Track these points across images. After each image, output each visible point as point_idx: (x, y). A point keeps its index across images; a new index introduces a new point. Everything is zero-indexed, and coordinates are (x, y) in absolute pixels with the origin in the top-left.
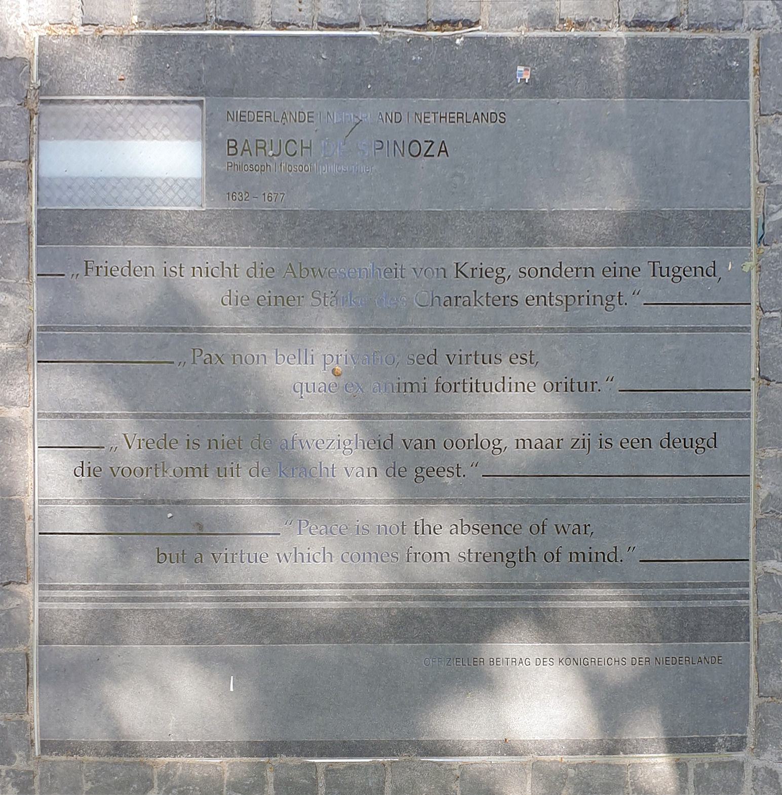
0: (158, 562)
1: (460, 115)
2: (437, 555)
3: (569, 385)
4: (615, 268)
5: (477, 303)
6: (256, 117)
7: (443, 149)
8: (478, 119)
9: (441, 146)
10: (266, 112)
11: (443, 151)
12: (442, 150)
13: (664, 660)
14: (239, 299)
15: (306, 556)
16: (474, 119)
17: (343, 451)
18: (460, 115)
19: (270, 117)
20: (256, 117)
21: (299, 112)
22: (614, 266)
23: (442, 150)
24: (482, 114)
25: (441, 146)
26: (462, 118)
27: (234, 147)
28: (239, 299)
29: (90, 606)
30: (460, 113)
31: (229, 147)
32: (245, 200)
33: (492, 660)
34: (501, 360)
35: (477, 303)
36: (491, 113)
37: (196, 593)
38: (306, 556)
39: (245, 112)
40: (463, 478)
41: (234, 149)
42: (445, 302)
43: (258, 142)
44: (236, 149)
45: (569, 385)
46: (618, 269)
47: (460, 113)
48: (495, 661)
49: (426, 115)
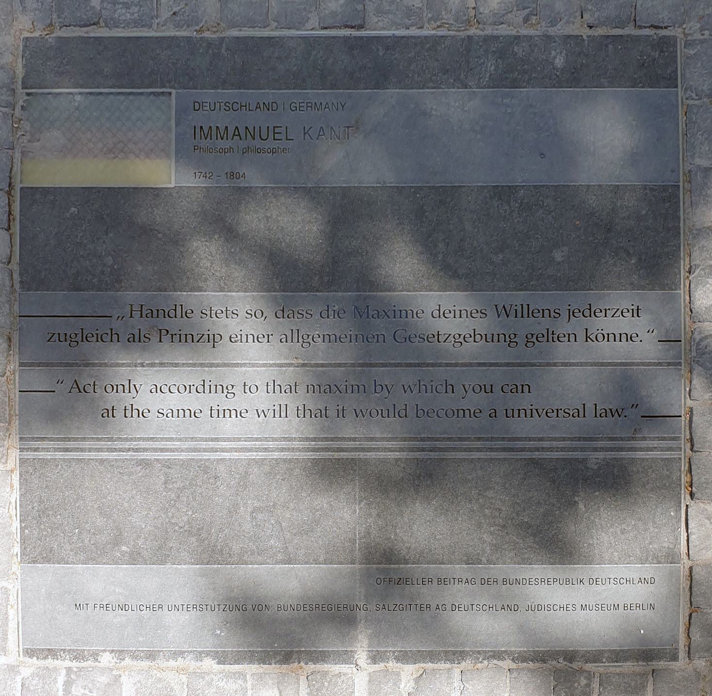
0: (417, 416)
1: (310, 105)
6: (201, 106)
7: (237, 133)
8: (260, 108)
9: (320, 130)
10: (307, 103)
11: (237, 135)
12: (236, 134)
15: (429, 387)
16: (257, 108)
17: (226, 395)
19: (311, 107)
20: (201, 106)
21: (272, 103)
23: (236, 134)
24: (264, 103)
25: (320, 130)
29: (412, 455)
34: (202, 312)
36: (272, 103)
37: (386, 444)
38: (429, 387)
39: (207, 102)
43: (276, 129)
48: (443, 581)
49: (301, 104)
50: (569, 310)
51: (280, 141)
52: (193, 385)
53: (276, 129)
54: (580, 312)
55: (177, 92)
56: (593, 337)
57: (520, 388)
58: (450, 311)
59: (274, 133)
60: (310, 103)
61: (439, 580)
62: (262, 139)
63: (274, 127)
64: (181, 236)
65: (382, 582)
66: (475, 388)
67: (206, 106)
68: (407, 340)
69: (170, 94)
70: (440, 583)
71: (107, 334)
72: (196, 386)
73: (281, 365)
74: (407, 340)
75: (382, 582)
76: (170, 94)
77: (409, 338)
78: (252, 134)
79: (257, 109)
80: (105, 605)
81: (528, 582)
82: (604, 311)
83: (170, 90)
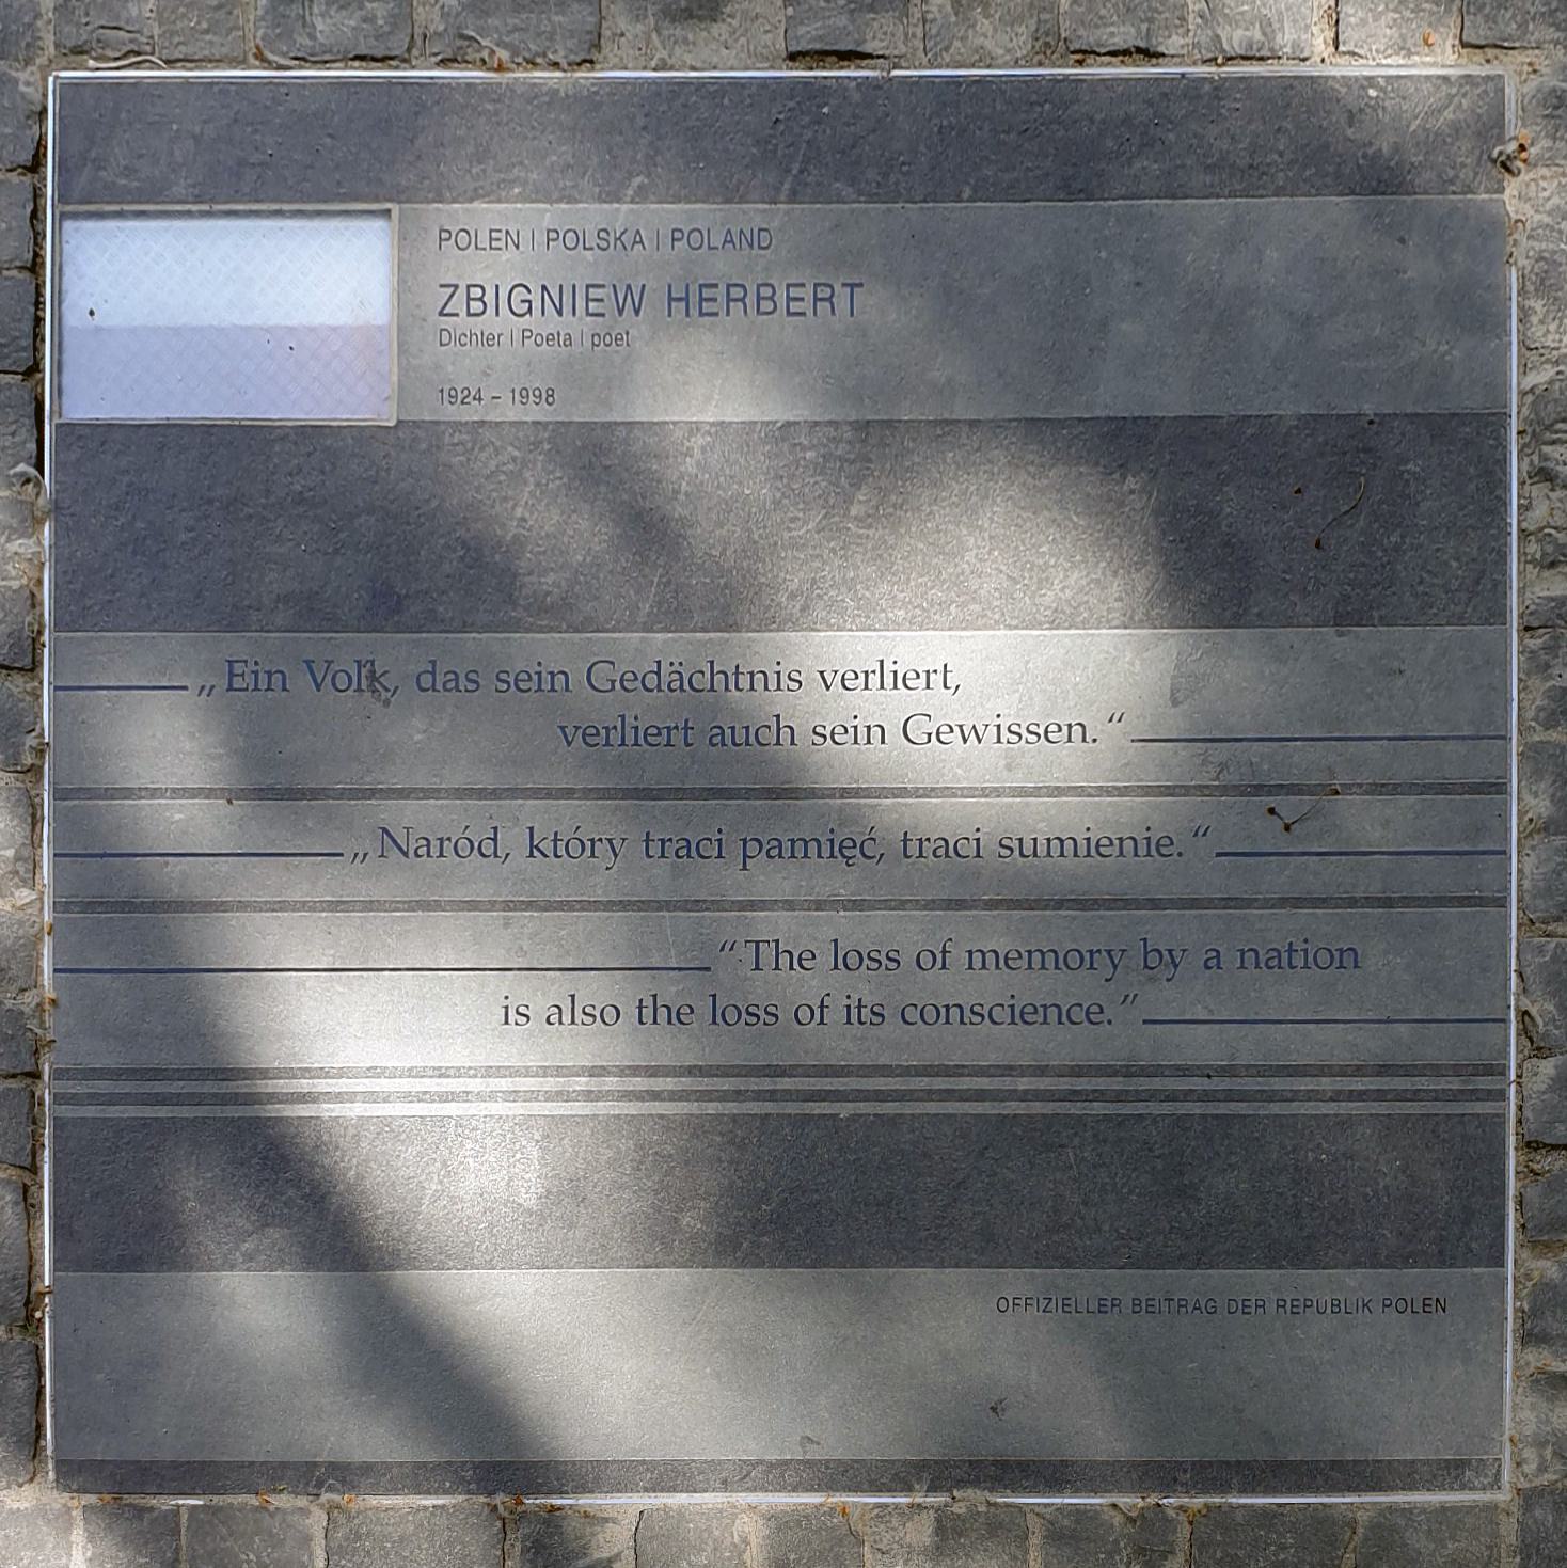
1: (737, 293)
2: (1247, 955)
3: (854, 1011)
4: (856, 727)
5: (536, 853)
8: (732, 241)
13: (1060, 1304)
14: (1093, 844)
18: (737, 293)
21: (760, 230)
22: (538, 669)
26: (742, 300)
27: (481, 299)
28: (1093, 844)
30: (736, 285)
31: (469, 299)
32: (462, 403)
33: (1336, 1303)
35: (536, 853)
39: (499, 231)
40: (1108, 1026)
41: (481, 304)
42: (768, 850)
43: (591, 290)
44: (485, 304)
45: (854, 1011)
46: (862, 731)
47: (736, 285)
50: (895, 673)
51: (455, 318)
52: (449, 839)
53: (732, 289)
54: (636, 679)
55: (400, 209)
56: (547, 846)
57: (435, 844)
58: (856, 673)
59: (588, 300)
60: (681, 231)
61: (1281, 1303)
62: (484, 312)
63: (588, 287)
64: (1094, 510)
65: (1011, 1308)
66: (459, 844)
67: (498, 240)
68: (933, 737)
69: (388, 212)
70: (1137, 1309)
71: (769, 727)
72: (453, 841)
73: (128, 793)
74: (933, 737)
75: (1011, 1308)
76: (388, 212)
77: (938, 733)
78: (629, 297)
79: (727, 245)
80: (1289, 1303)
81: (1240, 1307)
82: (862, 676)
83: (388, 205)
